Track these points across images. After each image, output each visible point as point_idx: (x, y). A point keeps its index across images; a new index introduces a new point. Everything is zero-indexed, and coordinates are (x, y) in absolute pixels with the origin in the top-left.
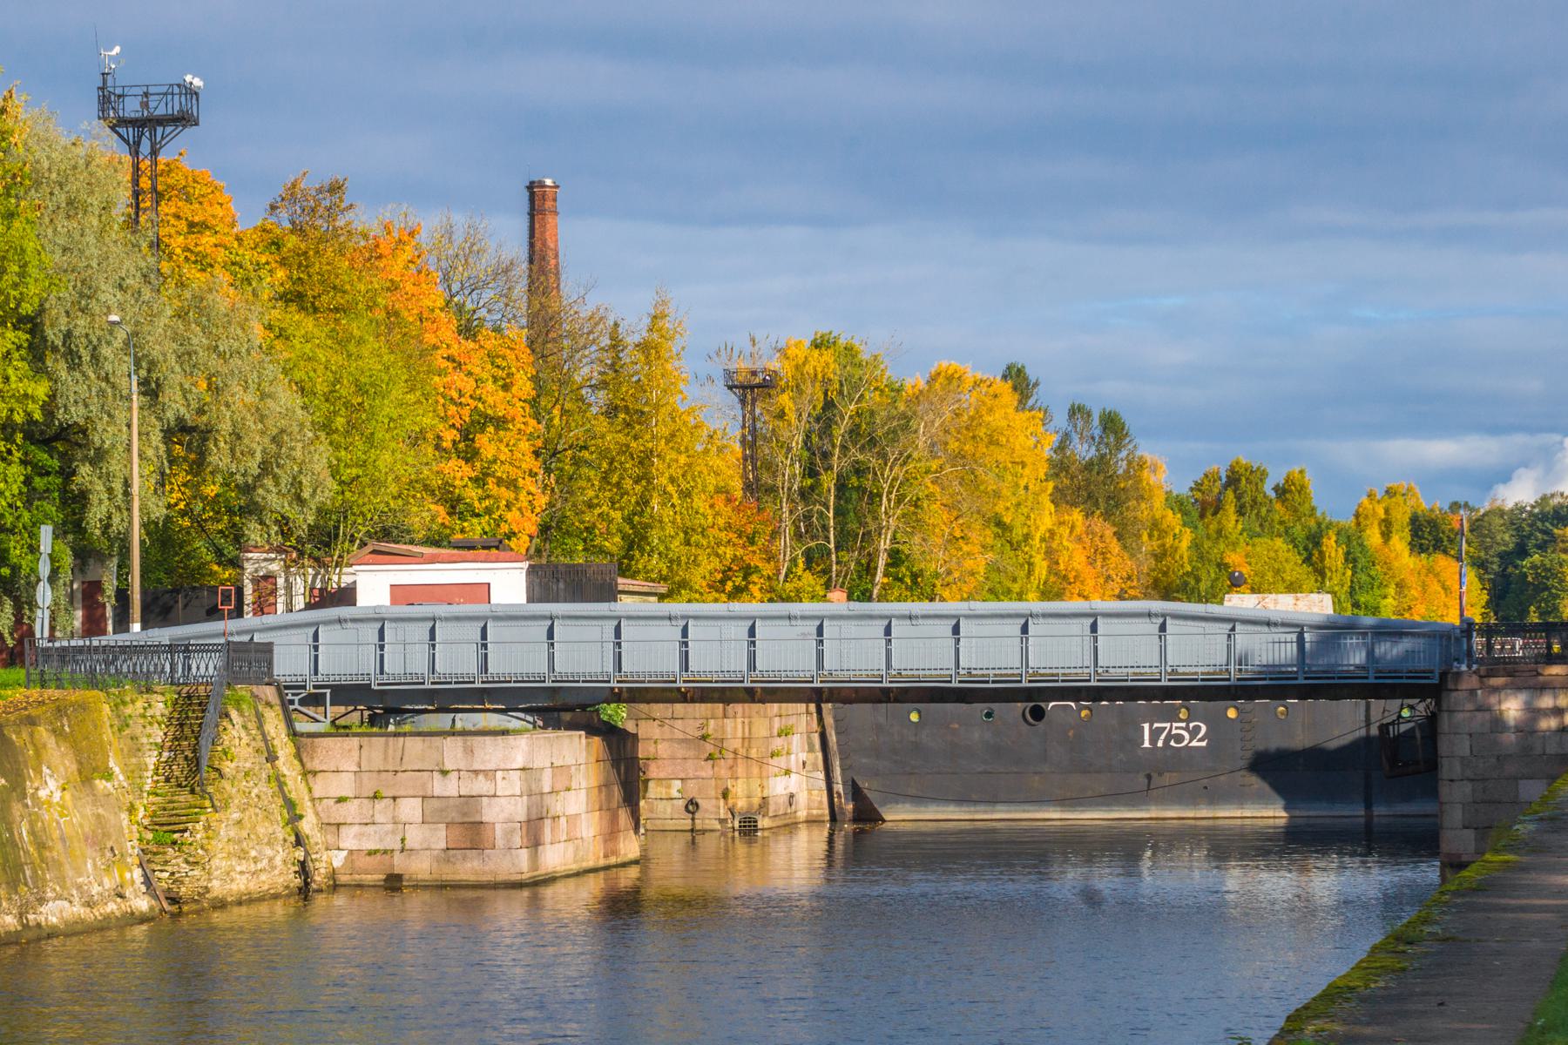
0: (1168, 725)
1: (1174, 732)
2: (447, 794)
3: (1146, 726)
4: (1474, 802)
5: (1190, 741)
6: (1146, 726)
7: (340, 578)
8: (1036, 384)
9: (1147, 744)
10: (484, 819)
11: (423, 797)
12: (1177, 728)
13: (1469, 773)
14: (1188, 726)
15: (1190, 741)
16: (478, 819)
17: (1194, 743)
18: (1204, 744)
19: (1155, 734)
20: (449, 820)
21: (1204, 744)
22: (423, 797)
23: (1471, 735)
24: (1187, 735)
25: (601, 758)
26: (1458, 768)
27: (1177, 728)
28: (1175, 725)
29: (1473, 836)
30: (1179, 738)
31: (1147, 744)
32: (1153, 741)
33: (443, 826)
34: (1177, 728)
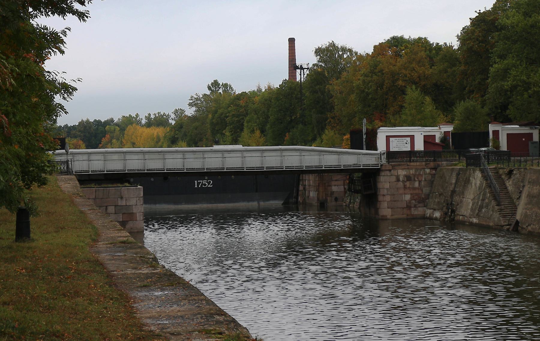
0: (202, 181)
1: (204, 183)
2: (122, 205)
3: (196, 181)
4: (391, 201)
5: (208, 186)
6: (196, 181)
7: (481, 29)
8: (137, 115)
9: (196, 186)
10: (134, 212)
11: (115, 206)
12: (205, 182)
13: (389, 193)
14: (207, 181)
15: (208, 186)
16: (132, 212)
17: (209, 186)
18: (212, 186)
19: (198, 184)
20: (123, 212)
21: (212, 186)
22: (115, 206)
23: (390, 182)
24: (207, 184)
25: (379, 202)
26: (385, 191)
27: (204, 182)
28: (204, 181)
29: (390, 211)
30: (205, 185)
31: (196, 186)
32: (198, 185)
33: (121, 214)
34: (204, 182)
